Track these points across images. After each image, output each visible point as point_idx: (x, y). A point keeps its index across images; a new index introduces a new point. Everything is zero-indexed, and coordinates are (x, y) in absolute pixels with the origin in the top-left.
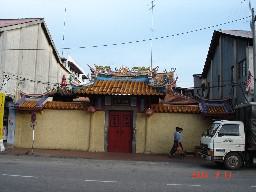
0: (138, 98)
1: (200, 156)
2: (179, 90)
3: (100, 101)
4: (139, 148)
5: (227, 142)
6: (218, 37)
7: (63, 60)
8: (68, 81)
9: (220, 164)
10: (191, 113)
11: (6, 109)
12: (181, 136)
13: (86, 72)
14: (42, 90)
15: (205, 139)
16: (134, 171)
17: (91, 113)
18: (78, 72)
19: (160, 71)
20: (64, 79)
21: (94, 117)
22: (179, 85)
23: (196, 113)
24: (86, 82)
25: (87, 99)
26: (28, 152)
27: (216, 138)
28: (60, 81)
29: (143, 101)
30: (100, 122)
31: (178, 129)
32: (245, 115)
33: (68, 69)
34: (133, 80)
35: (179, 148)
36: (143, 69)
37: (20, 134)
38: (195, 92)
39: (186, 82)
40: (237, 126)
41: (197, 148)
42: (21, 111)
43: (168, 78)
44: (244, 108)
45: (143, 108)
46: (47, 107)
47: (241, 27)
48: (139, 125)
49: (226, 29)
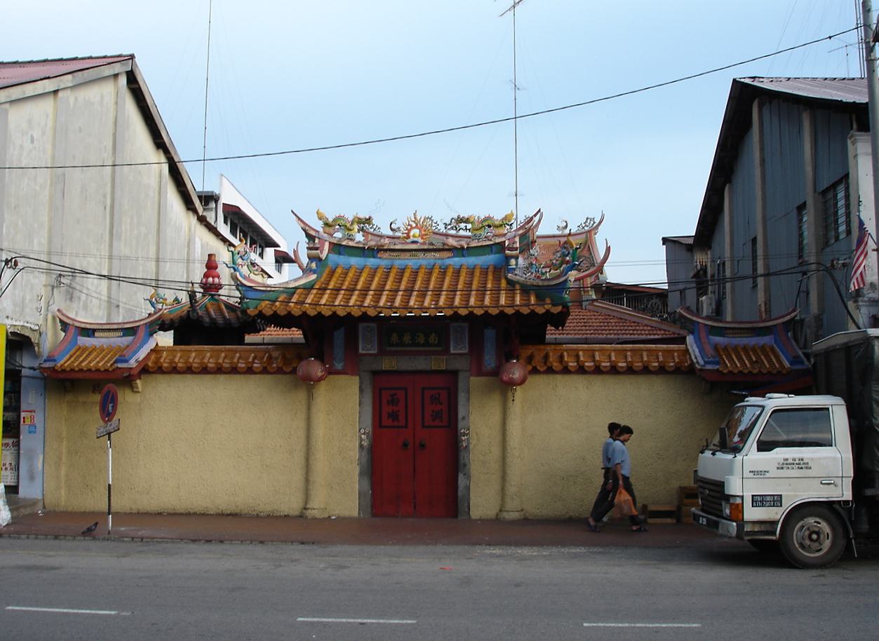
0: (476, 325)
1: (695, 521)
2: (616, 293)
3: (339, 336)
4: (482, 499)
5: (793, 467)
6: (747, 102)
7: (209, 199)
8: (224, 274)
9: (767, 550)
10: (662, 370)
11: (13, 376)
12: (629, 455)
13: (289, 238)
14: (137, 307)
15: (711, 464)
16: (466, 581)
17: (309, 383)
18: (260, 239)
19: (546, 228)
20: (211, 265)
21: (322, 391)
22: (615, 274)
23: (678, 371)
24: (288, 275)
25: (296, 334)
26: (89, 527)
27: (751, 456)
28: (198, 273)
29: (490, 334)
30: (339, 418)
31: (617, 431)
32: (846, 372)
33: (225, 230)
34: (456, 261)
35: (623, 496)
36: (488, 223)
37: (52, 460)
38: (673, 300)
39: (637, 262)
40: (374, 349)
41: (687, 494)
42: (66, 383)
43: (577, 250)
44: (848, 348)
45: (490, 360)
46: (154, 368)
47: (822, 55)
48: (480, 421)
49: (776, 72)
